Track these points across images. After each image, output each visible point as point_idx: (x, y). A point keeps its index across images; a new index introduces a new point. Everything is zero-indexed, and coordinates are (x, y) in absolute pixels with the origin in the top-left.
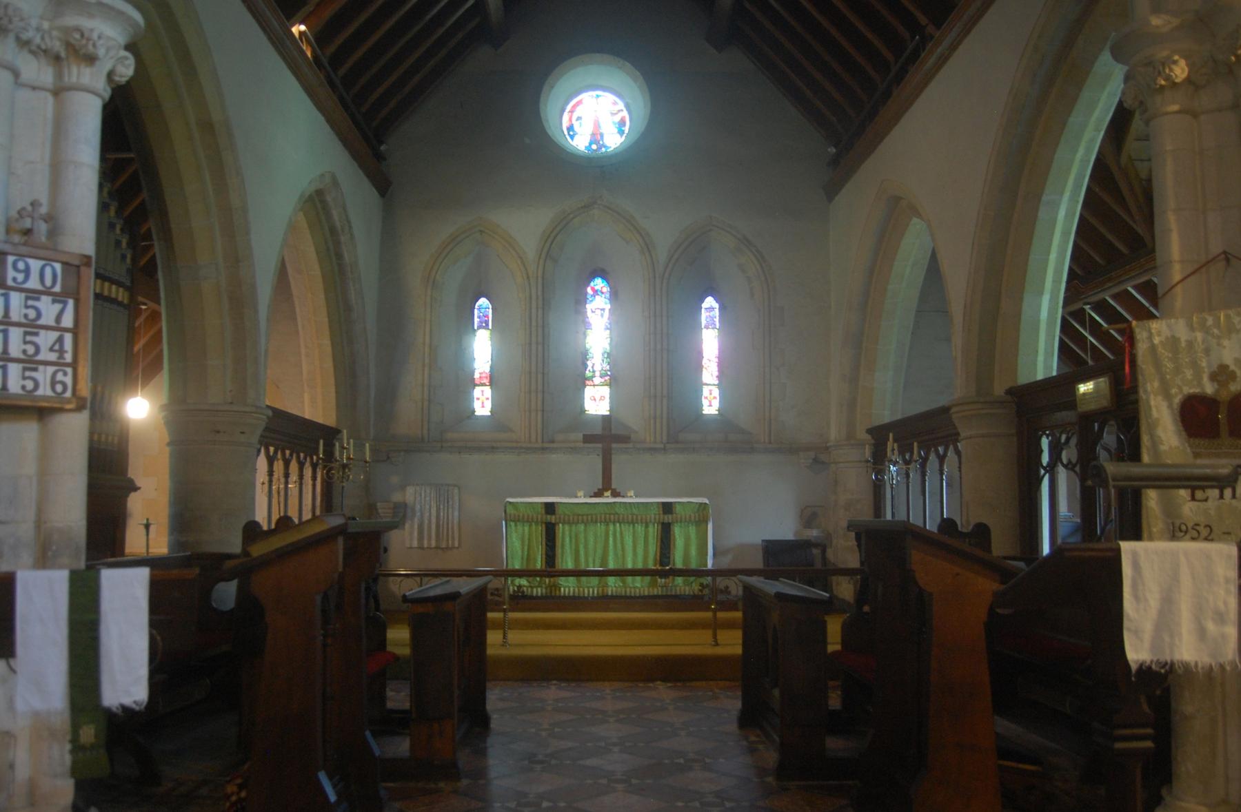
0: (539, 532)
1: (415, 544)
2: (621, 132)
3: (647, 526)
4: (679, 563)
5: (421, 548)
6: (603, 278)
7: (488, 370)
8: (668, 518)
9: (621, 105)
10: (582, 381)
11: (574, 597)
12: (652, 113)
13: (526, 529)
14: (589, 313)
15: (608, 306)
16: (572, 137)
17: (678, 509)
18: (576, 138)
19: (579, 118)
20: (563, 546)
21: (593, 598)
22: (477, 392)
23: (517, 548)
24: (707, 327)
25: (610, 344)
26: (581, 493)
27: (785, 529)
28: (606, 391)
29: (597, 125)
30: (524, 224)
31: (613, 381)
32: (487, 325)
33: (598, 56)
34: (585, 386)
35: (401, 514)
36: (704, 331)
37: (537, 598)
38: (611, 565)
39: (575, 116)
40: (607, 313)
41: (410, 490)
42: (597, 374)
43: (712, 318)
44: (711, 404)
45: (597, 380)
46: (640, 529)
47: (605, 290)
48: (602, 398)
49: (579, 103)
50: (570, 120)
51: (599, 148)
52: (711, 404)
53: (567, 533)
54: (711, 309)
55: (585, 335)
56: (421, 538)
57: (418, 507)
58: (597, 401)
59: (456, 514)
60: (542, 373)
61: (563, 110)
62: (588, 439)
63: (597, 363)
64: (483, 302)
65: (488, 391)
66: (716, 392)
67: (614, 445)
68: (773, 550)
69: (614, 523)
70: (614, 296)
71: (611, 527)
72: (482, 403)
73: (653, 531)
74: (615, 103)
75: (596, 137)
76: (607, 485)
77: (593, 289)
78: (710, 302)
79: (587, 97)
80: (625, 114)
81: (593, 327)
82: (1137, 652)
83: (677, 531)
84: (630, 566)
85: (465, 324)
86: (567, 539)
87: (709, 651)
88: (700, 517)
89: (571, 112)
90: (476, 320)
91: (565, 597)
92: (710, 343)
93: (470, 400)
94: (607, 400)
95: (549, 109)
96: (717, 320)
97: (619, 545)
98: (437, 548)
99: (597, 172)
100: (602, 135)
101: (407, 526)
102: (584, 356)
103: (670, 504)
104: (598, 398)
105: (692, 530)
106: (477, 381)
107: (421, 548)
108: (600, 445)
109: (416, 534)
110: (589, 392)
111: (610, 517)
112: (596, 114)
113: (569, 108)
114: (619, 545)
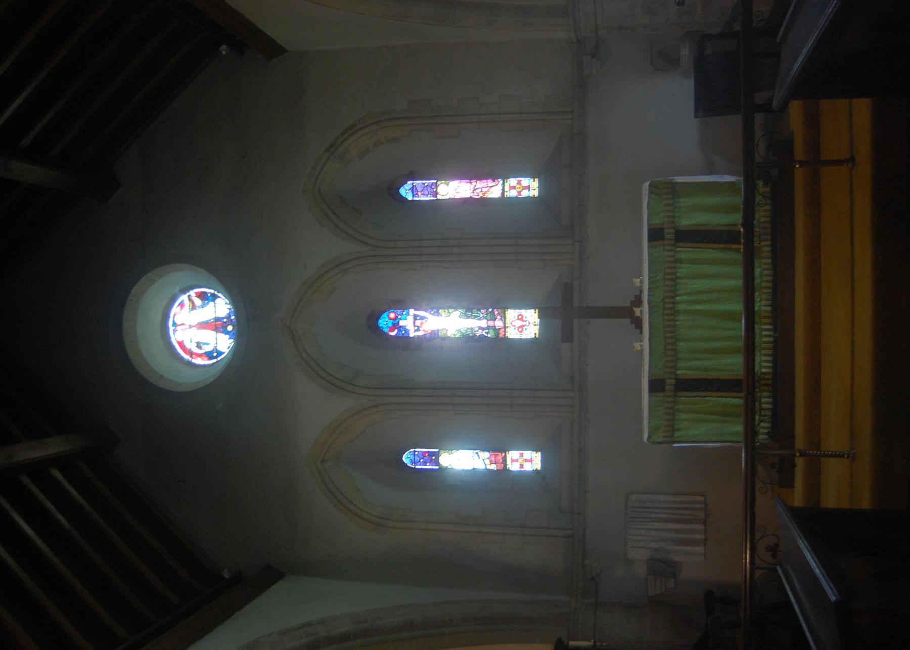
0: (686, 400)
1: (700, 549)
2: (214, 297)
3: (680, 261)
4: (737, 218)
5: (705, 542)
6: (379, 317)
7: (487, 455)
8: (669, 234)
9: (184, 298)
10: (499, 342)
11: (775, 356)
12: (185, 263)
13: (683, 416)
14: (420, 333)
15: (412, 311)
16: (220, 353)
17: (656, 221)
18: (220, 348)
19: (199, 345)
20: (706, 369)
21: (775, 330)
22: (514, 467)
23: (713, 428)
24: (436, 194)
25: (456, 309)
26: (637, 346)
27: (679, 90)
28: (511, 314)
29: (204, 325)
30: (314, 412)
31: (498, 304)
32: (433, 454)
33: (126, 325)
34: (505, 339)
35: (662, 567)
36: (439, 197)
37: (775, 403)
38: (738, 306)
39: (196, 350)
40: (421, 313)
41: (632, 554)
42: (491, 323)
43: (425, 187)
44: (528, 187)
45: (499, 324)
46: (683, 270)
47: (392, 315)
48: (521, 318)
49: (181, 344)
50: (199, 355)
51: (230, 322)
52: (528, 187)
53: (689, 363)
54: (413, 189)
55: (446, 338)
56: (692, 543)
57: (653, 545)
58: (523, 324)
59: (662, 498)
60: (487, 392)
61: (189, 364)
62: (567, 335)
63: (477, 324)
64: (406, 459)
65: (513, 454)
66: (513, 181)
67: (576, 303)
68: (708, 103)
69: (675, 303)
70: (401, 304)
71: (681, 307)
72: (526, 461)
73: (686, 252)
74: (182, 305)
75: (217, 325)
76: (626, 313)
77: (392, 329)
78: (405, 192)
79: (176, 337)
80: (192, 293)
81: (435, 328)
82: (539, 454)
83: (686, 222)
84: (739, 283)
85: (436, 481)
86: (698, 363)
87: (865, 169)
88: (667, 191)
89: (191, 354)
90: (428, 467)
91: (775, 367)
92: (454, 190)
93: (522, 475)
94: (523, 312)
95: (185, 381)
96: (427, 182)
97: (704, 297)
98: (705, 523)
99: (248, 323)
100: (217, 319)
101: (676, 558)
102: (469, 339)
103: (651, 231)
104: (520, 323)
105: (684, 202)
106: (501, 467)
107: (705, 542)
108: (576, 322)
109: (687, 548)
110: (512, 334)
111: (668, 308)
112: (196, 326)
113: (187, 357)
114: (704, 297)
